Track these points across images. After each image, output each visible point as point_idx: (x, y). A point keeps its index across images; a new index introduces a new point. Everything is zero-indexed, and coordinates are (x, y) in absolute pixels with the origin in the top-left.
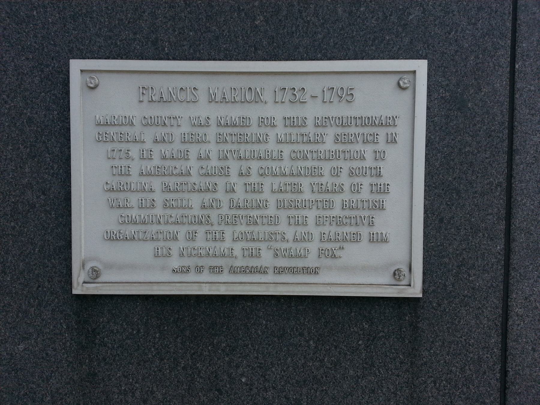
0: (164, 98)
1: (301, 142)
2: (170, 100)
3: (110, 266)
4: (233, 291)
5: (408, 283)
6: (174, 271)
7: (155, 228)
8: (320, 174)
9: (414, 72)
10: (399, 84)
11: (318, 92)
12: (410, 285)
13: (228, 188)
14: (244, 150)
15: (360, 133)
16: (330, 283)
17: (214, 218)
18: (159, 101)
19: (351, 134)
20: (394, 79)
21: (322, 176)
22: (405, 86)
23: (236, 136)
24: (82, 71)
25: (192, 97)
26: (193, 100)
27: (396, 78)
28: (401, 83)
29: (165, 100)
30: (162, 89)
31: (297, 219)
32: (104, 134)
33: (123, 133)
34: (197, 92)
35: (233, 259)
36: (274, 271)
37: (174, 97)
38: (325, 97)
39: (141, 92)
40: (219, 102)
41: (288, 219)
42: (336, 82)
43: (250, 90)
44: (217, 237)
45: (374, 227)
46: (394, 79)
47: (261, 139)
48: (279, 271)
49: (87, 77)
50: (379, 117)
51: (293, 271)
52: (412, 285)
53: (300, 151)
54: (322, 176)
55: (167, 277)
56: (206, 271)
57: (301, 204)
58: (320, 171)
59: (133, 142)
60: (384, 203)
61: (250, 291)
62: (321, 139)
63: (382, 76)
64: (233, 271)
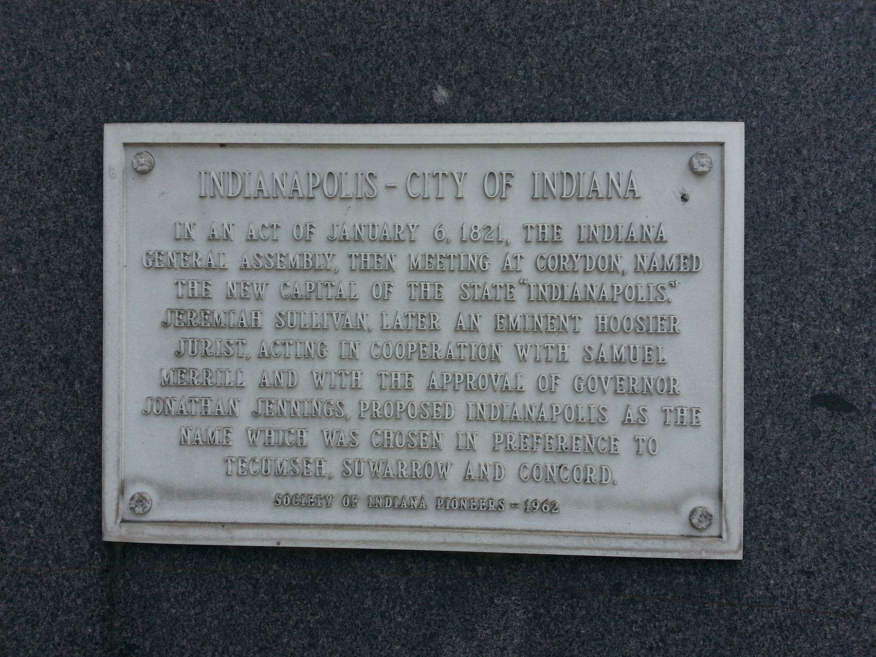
0: (265, 191)
1: (457, 269)
2: (275, 195)
3: (168, 492)
4: (715, 552)
5: (716, 533)
6: (278, 503)
7: (405, 426)
8: (432, 328)
9: (722, 144)
10: (690, 165)
11: (399, 179)
12: (720, 537)
13: (343, 352)
14: (610, 285)
15: (580, 255)
16: (572, 530)
17: (350, 409)
18: (290, 198)
19: (564, 257)
20: (683, 157)
21: (435, 330)
22: (701, 169)
23: (358, 260)
24: (125, 144)
25: (366, 188)
26: (368, 196)
27: (685, 155)
28: (696, 165)
29: (266, 195)
30: (296, 175)
31: (680, 414)
32: (157, 255)
33: (188, 254)
34: (375, 180)
35: (325, 480)
36: (435, 504)
37: (221, 189)
38: (536, 190)
39: (505, 183)
40: (252, 198)
41: (662, 415)
42: (427, 163)
43: (492, 177)
44: (273, 441)
45: (644, 428)
46: (683, 157)
47: (475, 264)
48: (373, 504)
49: (133, 151)
50: (657, 225)
51: (397, 504)
52: (724, 536)
53: (630, 287)
54: (435, 330)
55: (263, 513)
56: (361, 506)
57: (476, 383)
58: (432, 322)
59: (206, 269)
60: (359, 378)
61: (671, 551)
62: (571, 266)
63: (557, 150)
64: (444, 504)
